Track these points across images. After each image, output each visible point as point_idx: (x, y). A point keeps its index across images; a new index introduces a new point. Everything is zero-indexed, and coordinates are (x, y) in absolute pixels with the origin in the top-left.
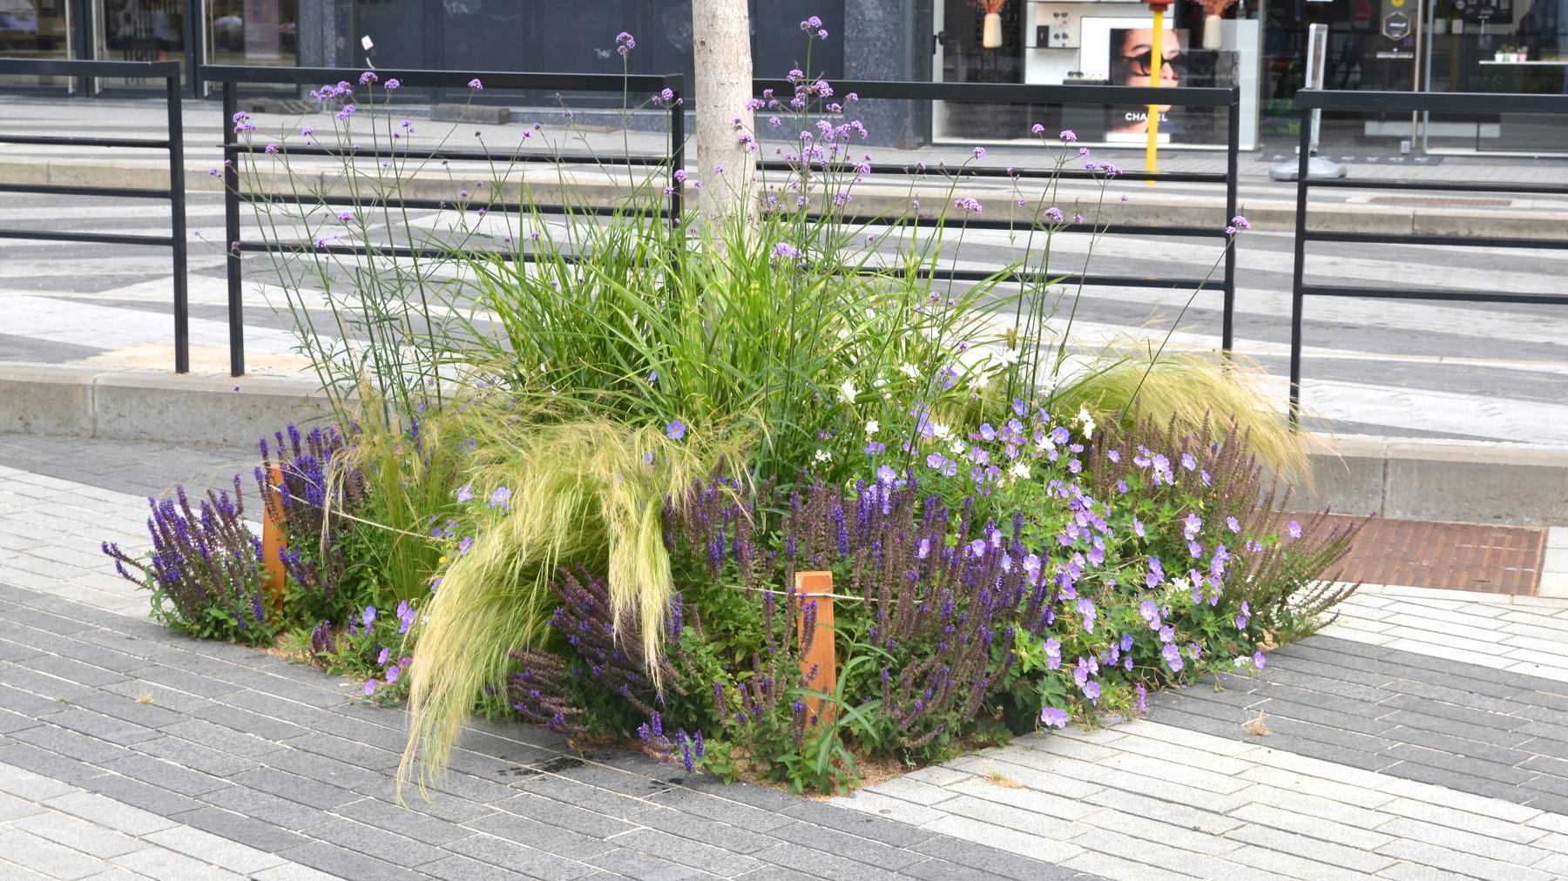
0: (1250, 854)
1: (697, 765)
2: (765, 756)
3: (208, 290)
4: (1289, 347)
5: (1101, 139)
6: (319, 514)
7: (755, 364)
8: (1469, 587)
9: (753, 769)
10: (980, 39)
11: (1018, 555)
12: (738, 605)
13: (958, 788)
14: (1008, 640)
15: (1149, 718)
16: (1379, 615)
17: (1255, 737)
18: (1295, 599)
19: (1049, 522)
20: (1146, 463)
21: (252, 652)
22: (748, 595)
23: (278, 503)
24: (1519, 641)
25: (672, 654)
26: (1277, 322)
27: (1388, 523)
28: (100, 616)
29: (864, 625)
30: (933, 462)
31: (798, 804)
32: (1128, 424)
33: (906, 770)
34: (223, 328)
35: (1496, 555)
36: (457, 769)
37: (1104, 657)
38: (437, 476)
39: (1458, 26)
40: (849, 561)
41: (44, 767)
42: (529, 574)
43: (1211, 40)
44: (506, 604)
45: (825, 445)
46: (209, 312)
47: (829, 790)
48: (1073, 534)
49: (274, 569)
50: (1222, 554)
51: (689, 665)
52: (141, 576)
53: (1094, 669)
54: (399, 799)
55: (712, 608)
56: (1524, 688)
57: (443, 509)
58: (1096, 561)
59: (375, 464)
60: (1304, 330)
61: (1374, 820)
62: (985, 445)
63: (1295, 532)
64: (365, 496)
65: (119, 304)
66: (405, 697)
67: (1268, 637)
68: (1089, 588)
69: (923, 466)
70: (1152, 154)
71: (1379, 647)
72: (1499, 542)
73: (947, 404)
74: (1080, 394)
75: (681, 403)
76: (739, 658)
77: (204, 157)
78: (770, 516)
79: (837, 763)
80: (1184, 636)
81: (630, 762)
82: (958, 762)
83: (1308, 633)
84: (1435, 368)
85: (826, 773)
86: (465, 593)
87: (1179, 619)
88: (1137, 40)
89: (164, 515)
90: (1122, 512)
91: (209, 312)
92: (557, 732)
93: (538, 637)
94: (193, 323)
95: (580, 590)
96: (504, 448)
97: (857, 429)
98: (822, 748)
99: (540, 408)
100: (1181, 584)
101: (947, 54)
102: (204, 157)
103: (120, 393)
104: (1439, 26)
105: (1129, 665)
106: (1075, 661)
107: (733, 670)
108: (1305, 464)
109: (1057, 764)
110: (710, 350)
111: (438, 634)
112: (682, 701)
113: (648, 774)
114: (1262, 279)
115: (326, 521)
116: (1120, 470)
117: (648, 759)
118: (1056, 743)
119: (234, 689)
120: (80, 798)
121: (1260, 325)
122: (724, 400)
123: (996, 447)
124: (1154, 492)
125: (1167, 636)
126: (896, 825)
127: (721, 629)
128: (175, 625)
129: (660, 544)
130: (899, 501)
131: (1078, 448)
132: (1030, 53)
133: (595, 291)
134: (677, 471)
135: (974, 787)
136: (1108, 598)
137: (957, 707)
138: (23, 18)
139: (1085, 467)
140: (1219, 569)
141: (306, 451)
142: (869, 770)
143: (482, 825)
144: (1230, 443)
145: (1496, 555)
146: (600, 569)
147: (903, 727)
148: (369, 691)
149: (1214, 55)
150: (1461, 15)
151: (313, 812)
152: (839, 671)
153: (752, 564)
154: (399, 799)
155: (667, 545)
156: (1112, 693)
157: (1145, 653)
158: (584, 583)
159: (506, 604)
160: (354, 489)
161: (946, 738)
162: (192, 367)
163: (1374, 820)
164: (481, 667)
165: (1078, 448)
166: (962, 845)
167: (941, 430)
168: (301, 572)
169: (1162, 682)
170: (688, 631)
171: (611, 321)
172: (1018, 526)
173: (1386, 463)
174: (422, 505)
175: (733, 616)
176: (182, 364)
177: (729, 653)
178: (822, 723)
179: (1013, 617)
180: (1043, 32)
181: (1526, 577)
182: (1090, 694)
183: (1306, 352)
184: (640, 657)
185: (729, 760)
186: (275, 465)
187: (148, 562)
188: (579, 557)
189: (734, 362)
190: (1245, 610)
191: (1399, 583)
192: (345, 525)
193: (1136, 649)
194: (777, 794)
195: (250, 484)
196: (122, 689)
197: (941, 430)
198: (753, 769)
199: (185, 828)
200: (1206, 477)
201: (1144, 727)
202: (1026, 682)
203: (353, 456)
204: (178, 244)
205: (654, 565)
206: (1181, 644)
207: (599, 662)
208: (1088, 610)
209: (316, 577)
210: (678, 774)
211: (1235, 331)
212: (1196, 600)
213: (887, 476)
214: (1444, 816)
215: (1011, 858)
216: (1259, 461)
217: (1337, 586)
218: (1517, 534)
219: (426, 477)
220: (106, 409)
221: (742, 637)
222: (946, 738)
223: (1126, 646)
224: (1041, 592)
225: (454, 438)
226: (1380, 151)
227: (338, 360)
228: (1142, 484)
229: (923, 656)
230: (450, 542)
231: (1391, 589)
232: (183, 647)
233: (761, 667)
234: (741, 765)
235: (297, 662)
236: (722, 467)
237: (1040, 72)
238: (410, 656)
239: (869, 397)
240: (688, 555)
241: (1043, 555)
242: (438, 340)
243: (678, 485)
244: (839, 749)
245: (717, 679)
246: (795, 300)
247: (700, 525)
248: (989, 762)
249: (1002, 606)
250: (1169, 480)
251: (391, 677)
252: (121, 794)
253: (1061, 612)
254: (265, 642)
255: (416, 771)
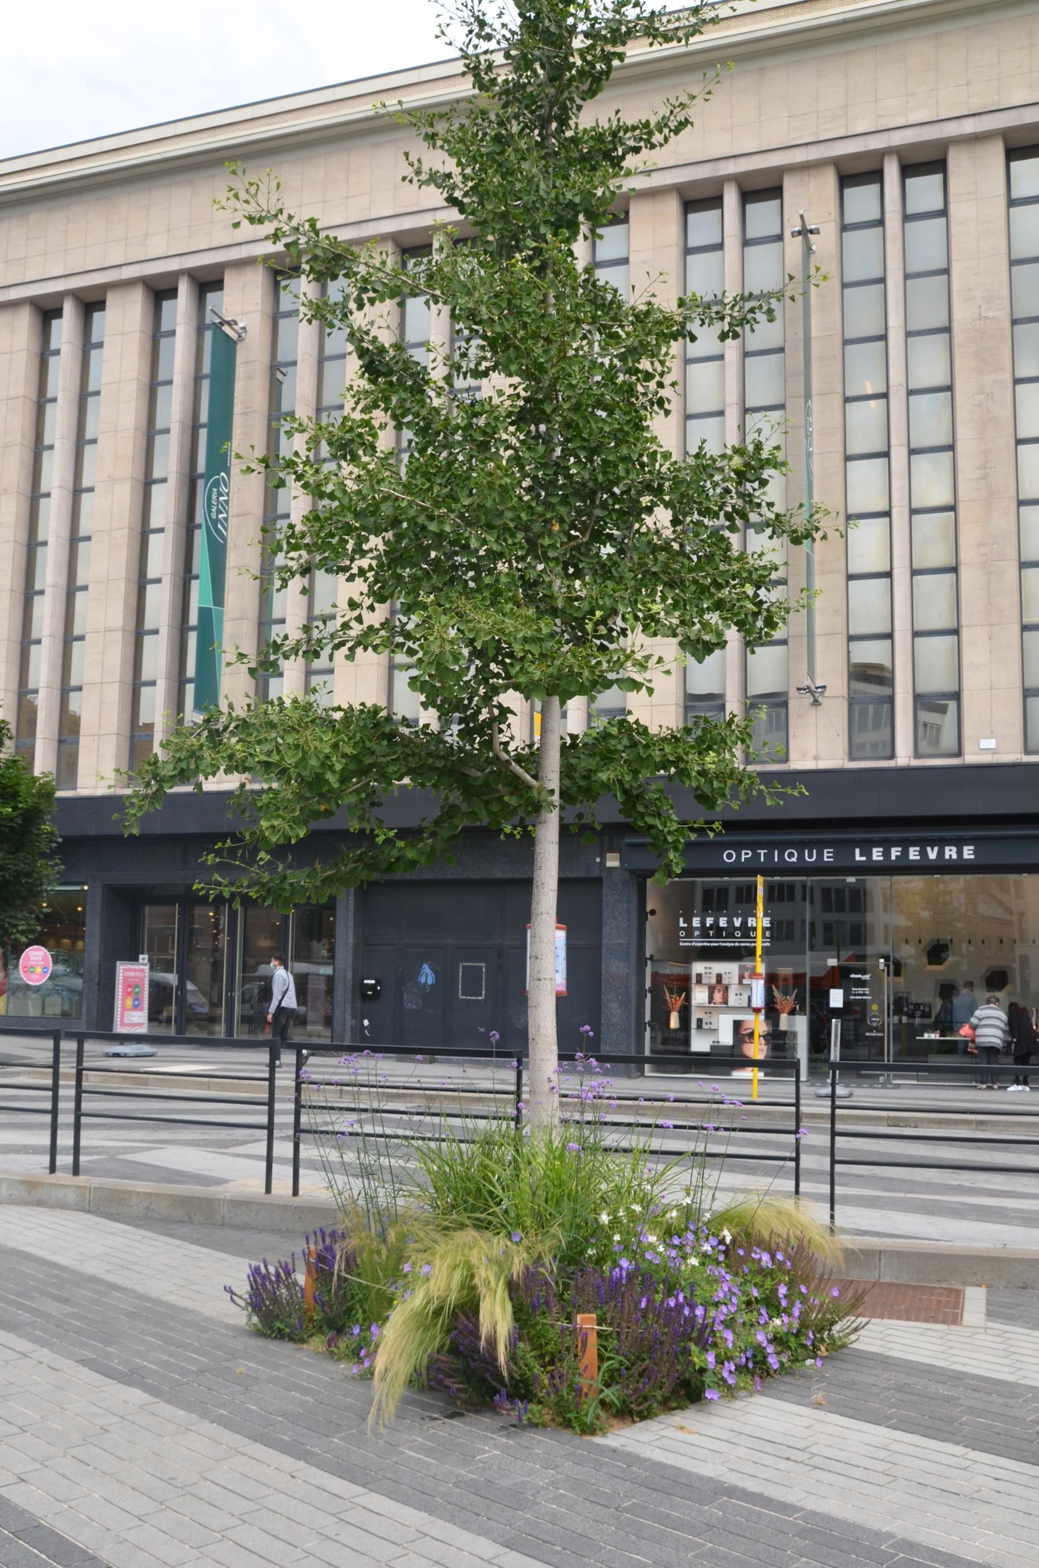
0: (817, 1473)
1: (524, 1418)
2: (561, 1414)
3: (283, 1149)
4: (828, 1187)
5: (729, 1074)
6: (332, 1274)
7: (558, 1203)
8: (926, 1321)
9: (553, 1420)
10: (668, 1023)
11: (692, 1307)
12: (547, 1331)
13: (663, 1433)
14: (687, 1352)
15: (762, 1394)
16: (880, 1336)
17: (818, 1406)
18: (837, 1328)
19: (708, 1288)
20: (757, 1257)
21: (296, 1346)
22: (552, 1326)
23: (313, 1268)
24: (954, 1351)
25: (512, 1357)
26: (821, 1173)
27: (882, 1284)
28: (220, 1323)
29: (613, 1343)
30: (648, 1256)
31: (577, 1441)
32: (748, 1235)
33: (634, 1422)
34: (290, 1170)
35: (939, 1302)
36: (400, 1416)
37: (737, 1360)
38: (394, 1257)
39: (905, 1019)
40: (605, 1309)
41: (189, 1407)
42: (438, 1312)
43: (783, 1026)
44: (426, 1328)
45: (592, 1245)
46: (283, 1161)
47: (593, 1433)
48: (721, 1295)
49: (309, 1303)
50: (798, 1305)
51: (521, 1363)
52: (243, 1304)
53: (733, 1368)
54: (369, 1433)
55: (533, 1332)
56: (957, 1378)
57: (395, 1272)
58: (733, 1309)
59: (362, 1249)
60: (836, 1177)
61: (883, 1454)
62: (675, 1247)
63: (836, 1293)
64: (357, 1266)
65: (239, 1156)
66: (372, 1374)
67: (823, 1349)
68: (729, 1324)
69: (643, 1256)
70: (755, 1082)
71: (881, 1355)
72: (940, 1295)
73: (655, 1224)
74: (723, 1218)
75: (519, 1223)
76: (547, 1359)
77: (285, 1079)
78: (564, 1283)
79: (598, 1417)
80: (779, 1349)
81: (489, 1415)
82: (662, 1418)
83: (844, 1346)
84: (904, 1199)
85: (592, 1423)
86: (404, 1322)
87: (777, 1340)
88: (746, 1026)
89: (256, 1271)
90: (746, 1282)
91: (283, 1161)
92: (452, 1399)
93: (442, 1346)
94: (275, 1166)
95: (466, 1322)
96: (428, 1243)
97: (609, 1238)
98: (590, 1410)
99: (447, 1223)
100: (778, 1322)
101: (652, 1030)
102: (285, 1079)
103: (236, 1204)
104: (896, 1018)
105: (751, 1365)
106: (722, 1363)
107: (544, 1366)
108: (840, 1255)
109: (714, 1420)
110: (534, 1194)
111: (390, 1344)
112: (517, 1382)
113: (499, 1422)
114: (814, 1150)
115: (335, 1278)
116: (744, 1260)
117: (498, 1414)
118: (713, 1408)
119: (286, 1367)
120: (206, 1425)
121: (814, 1175)
122: (542, 1223)
123: (680, 1247)
124: (762, 1271)
125: (770, 1349)
126: (629, 1454)
127: (538, 1345)
128: (258, 1330)
129: (507, 1298)
130: (631, 1277)
131: (722, 1248)
132: (693, 1031)
133: (476, 1162)
134: (516, 1260)
135: (670, 1432)
136: (739, 1329)
137: (661, 1388)
138: (202, 1006)
139: (726, 1257)
140: (797, 1313)
141: (328, 1240)
142: (615, 1422)
143: (411, 1449)
144: (801, 1247)
145: (939, 1302)
146: (476, 1312)
147: (633, 1399)
148: (355, 1371)
149: (785, 1033)
150: (906, 1014)
151: (324, 1438)
152: (599, 1368)
153: (555, 1309)
154: (369, 1433)
155: (511, 1299)
156: (743, 1380)
157: (759, 1358)
158: (468, 1318)
159: (426, 1328)
160: (351, 1261)
161: (655, 1405)
162: (273, 1191)
163: (883, 1454)
164: (413, 1361)
165: (722, 1248)
166: (664, 1466)
167: (653, 1239)
168: (323, 1305)
169: (768, 1374)
170: (521, 1345)
171: (484, 1178)
172: (692, 1291)
173: (880, 1252)
174: (384, 1270)
175: (544, 1337)
176: (268, 1189)
177: (542, 1356)
178: (590, 1396)
179: (690, 1339)
180: (700, 1021)
181: (955, 1315)
182: (730, 1381)
183: (839, 1190)
184: (495, 1359)
185: (541, 1415)
186: (312, 1247)
187: (247, 1296)
188: (465, 1304)
189: (546, 1202)
190: (811, 1335)
191: (890, 1317)
192: (346, 1280)
193: (754, 1356)
194: (566, 1435)
195: (299, 1256)
196: (229, 1364)
197: (653, 1239)
198: (553, 1420)
199: (258, 1445)
200: (789, 1264)
201: (760, 1400)
202: (697, 1375)
203: (353, 1242)
204: (270, 1127)
205: (504, 1310)
206: (778, 1353)
207: (475, 1361)
208: (729, 1336)
209: (331, 1308)
210: (514, 1422)
211: (801, 1178)
212: (785, 1329)
213: (624, 1263)
214: (919, 1452)
215: (690, 1475)
216: (816, 1255)
217: (860, 1319)
218: (949, 1290)
219: (388, 1258)
220: (230, 1212)
221: (549, 1348)
222: (655, 1405)
223: (749, 1354)
224: (705, 1326)
225: (403, 1238)
226: (869, 1081)
227: (346, 1194)
228: (755, 1268)
229: (643, 1360)
230: (399, 1292)
231: (886, 1321)
232: (261, 1342)
233: (558, 1364)
234: (547, 1418)
235: (318, 1353)
236: (540, 1257)
237: (700, 1044)
238: (376, 1352)
239: (615, 1223)
240: (521, 1304)
241: (706, 1305)
242: (396, 1177)
243: (517, 1268)
244: (599, 1411)
245: (535, 1371)
246: (578, 1171)
247: (528, 1288)
248: (679, 1418)
249: (684, 1333)
250: (770, 1265)
251: (367, 1364)
252: (226, 1423)
253: (714, 1336)
254: (303, 1341)
255: (378, 1417)
